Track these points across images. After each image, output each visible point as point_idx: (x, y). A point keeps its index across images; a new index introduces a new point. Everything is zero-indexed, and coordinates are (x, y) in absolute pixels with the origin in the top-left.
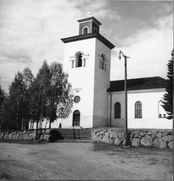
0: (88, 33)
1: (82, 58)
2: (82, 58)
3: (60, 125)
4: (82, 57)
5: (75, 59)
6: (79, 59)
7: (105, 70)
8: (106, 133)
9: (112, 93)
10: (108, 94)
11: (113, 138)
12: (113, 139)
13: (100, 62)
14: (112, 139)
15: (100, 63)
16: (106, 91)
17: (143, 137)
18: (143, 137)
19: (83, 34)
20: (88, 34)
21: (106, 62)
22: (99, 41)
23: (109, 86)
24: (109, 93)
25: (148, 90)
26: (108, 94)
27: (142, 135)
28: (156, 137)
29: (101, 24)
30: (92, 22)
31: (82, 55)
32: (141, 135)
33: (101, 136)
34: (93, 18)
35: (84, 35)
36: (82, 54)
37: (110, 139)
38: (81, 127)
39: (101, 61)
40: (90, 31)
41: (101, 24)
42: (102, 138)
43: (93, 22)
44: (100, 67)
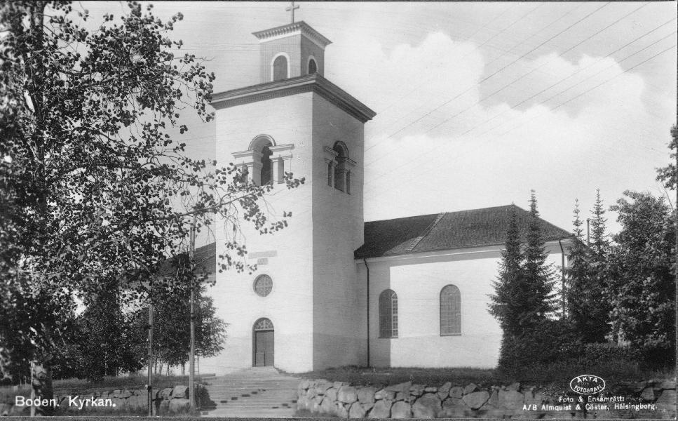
0: (289, 77)
1: (271, 157)
2: (271, 157)
3: (123, 18)
4: (271, 153)
5: (250, 159)
6: (262, 160)
7: (345, 190)
8: (329, 391)
9: (368, 260)
10: (357, 264)
11: (346, 404)
12: (347, 406)
13: (330, 166)
14: (344, 406)
15: (330, 173)
16: (353, 258)
17: (418, 397)
18: (418, 397)
19: (272, 80)
20: (291, 79)
21: (347, 167)
22: (320, 98)
23: (360, 241)
24: (361, 261)
25: (484, 251)
26: (357, 264)
27: (416, 393)
28: (449, 396)
29: (330, 42)
30: (300, 37)
31: (270, 148)
32: (413, 393)
33: (319, 398)
34: (301, 26)
35: (275, 82)
36: (270, 144)
37: (341, 405)
38: (277, 369)
39: (331, 162)
40: (293, 70)
41: (330, 42)
42: (320, 404)
43: (302, 35)
44: (329, 184)
